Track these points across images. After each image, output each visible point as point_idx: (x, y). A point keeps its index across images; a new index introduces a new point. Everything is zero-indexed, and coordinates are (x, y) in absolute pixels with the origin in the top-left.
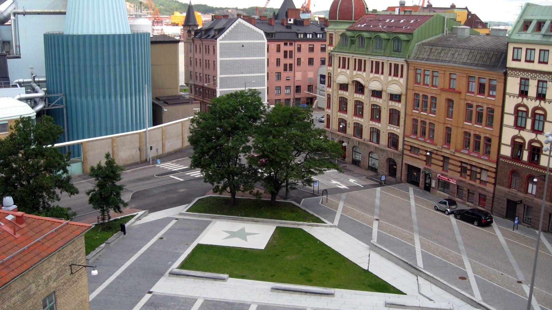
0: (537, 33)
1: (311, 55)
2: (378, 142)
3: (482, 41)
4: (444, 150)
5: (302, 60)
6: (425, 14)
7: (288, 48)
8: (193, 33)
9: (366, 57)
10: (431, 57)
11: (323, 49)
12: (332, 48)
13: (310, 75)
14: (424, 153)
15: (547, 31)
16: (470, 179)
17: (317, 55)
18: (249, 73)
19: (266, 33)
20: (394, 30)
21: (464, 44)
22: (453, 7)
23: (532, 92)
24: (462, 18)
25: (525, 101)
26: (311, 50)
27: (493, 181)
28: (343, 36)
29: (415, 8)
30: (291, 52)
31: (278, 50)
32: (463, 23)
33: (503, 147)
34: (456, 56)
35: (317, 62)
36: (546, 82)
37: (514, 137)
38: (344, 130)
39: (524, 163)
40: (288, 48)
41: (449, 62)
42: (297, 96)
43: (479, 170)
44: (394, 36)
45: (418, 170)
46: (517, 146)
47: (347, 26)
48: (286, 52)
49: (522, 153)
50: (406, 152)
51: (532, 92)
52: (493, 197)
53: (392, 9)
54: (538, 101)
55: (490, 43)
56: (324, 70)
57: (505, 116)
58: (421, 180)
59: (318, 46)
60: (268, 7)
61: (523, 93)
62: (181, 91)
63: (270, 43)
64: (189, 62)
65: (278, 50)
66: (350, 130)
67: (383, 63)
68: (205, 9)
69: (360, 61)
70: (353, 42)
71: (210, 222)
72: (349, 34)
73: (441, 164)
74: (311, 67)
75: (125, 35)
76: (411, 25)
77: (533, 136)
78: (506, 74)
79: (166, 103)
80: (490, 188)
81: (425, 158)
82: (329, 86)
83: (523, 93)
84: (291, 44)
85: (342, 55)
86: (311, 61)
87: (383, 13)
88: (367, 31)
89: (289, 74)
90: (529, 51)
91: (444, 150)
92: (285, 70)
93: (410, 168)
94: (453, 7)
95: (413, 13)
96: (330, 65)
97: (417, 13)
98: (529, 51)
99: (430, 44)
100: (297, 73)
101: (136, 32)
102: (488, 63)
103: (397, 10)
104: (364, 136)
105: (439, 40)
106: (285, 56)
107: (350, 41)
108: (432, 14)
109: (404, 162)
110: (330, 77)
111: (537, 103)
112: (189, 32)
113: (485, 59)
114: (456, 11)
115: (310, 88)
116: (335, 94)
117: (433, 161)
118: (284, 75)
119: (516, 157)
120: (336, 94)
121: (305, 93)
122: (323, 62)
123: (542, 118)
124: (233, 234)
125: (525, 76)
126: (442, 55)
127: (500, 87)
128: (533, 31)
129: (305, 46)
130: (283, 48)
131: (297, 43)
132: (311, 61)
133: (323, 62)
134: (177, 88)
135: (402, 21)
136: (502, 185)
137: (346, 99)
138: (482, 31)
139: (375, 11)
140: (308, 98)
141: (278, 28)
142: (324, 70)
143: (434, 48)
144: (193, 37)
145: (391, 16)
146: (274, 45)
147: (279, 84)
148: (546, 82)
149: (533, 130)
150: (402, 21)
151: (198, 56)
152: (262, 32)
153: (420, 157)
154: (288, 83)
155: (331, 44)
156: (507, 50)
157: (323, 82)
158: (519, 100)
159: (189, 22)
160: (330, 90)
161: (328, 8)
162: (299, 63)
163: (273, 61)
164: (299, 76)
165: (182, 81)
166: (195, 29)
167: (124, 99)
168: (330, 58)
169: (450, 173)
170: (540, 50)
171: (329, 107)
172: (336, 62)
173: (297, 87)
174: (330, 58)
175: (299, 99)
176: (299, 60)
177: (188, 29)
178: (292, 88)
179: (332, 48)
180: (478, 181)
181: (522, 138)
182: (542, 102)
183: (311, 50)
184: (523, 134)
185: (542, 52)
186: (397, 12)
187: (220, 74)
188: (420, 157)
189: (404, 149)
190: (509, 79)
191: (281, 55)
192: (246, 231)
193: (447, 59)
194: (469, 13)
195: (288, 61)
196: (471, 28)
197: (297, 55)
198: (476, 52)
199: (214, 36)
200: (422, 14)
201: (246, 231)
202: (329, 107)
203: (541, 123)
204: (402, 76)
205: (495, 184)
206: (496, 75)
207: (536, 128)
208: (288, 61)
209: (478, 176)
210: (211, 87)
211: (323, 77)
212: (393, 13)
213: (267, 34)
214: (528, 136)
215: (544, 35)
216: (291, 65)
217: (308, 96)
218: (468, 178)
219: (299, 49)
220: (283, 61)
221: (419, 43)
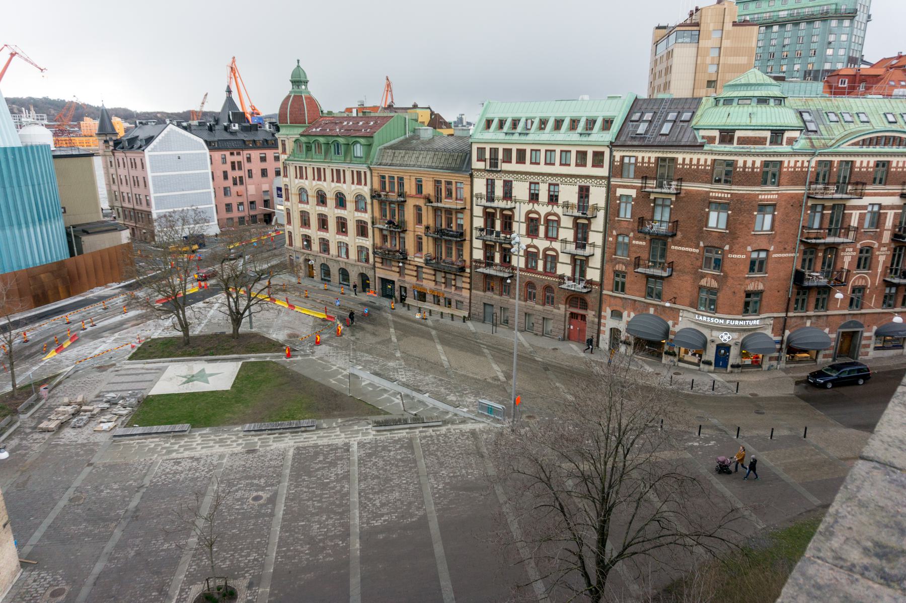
0: (572, 132)
1: (264, 165)
2: (348, 257)
3: (446, 142)
4: (416, 259)
5: (254, 172)
6: (385, 115)
7: (236, 158)
8: (111, 143)
9: (325, 165)
10: (394, 162)
11: (277, 159)
12: (285, 157)
13: (265, 187)
14: (396, 264)
15: (509, 128)
16: (446, 287)
17: (271, 166)
18: (191, 189)
19: (206, 141)
20: (353, 133)
21: (428, 146)
22: (415, 106)
23: (543, 196)
24: (425, 117)
25: (537, 207)
26: (263, 159)
27: (468, 286)
28: (296, 141)
29: (375, 108)
30: (239, 163)
31: (224, 162)
32: (426, 124)
33: (475, 251)
34: (420, 159)
35: (271, 173)
36: (558, 185)
37: (528, 246)
38: (309, 246)
39: (539, 273)
40: (236, 158)
41: (414, 166)
42: (253, 213)
43: (453, 277)
44: (354, 140)
45: (393, 282)
46: (531, 256)
47: (301, 130)
48: (233, 163)
49: (536, 263)
50: (378, 265)
51: (543, 196)
52: (470, 303)
53: (349, 110)
54: (550, 206)
55: (454, 144)
56: (281, 181)
57: (474, 218)
58: (397, 294)
59: (270, 154)
60: (206, 109)
61: (534, 198)
62: (104, 216)
63: (212, 153)
64: (112, 181)
65: (224, 162)
66: (316, 247)
67: (344, 171)
68: (127, 115)
69: (338, 171)
70: (309, 149)
71: (167, 367)
72: (303, 139)
73: (415, 274)
74: (265, 179)
75: (13, 149)
76: (371, 128)
77: (547, 244)
78: (471, 176)
79: (86, 232)
80: (466, 293)
81: (397, 270)
82: (287, 199)
83: (534, 198)
84: (238, 154)
85: (298, 164)
86: (264, 173)
87: (339, 115)
88: (323, 136)
89: (239, 188)
90: (534, 153)
91: (416, 259)
92: (235, 184)
93: (385, 282)
94: (415, 106)
95: (372, 115)
96: (285, 176)
97: (377, 115)
98: (564, 154)
99: (392, 147)
100: (249, 187)
101: (29, 144)
102: (453, 165)
103: (354, 111)
104: (331, 252)
105: (402, 142)
106: (233, 168)
107: (307, 147)
108: (392, 114)
109: (377, 275)
110: (287, 190)
111: (549, 209)
112: (106, 142)
113: (450, 161)
114: (418, 111)
115: (266, 203)
116: (295, 208)
117: (407, 272)
118: (234, 189)
119: (530, 268)
120: (297, 208)
121: (261, 209)
122: (278, 173)
123: (555, 225)
124: (190, 379)
125: (554, 182)
126: (406, 159)
127: (467, 188)
128: (496, 129)
129: (255, 154)
130: (230, 159)
131: (245, 152)
132: (264, 173)
133: (278, 173)
134: (97, 212)
135: (361, 123)
136: (477, 289)
137: (326, 216)
138: (445, 132)
139: (330, 113)
140: (265, 215)
141: (220, 135)
142: (281, 181)
143: (397, 152)
144: (112, 148)
145: (349, 118)
146: (218, 155)
147: (228, 200)
148: (558, 185)
149: (547, 237)
150: (361, 123)
151: (122, 172)
152: (202, 141)
153: (394, 269)
154: (240, 200)
155: (284, 152)
156: (471, 151)
157: (280, 196)
158: (530, 207)
159: (106, 129)
160: (288, 204)
161: (277, 111)
162: (250, 176)
163: (219, 174)
164: (252, 189)
165: (105, 204)
166: (114, 138)
167: (24, 230)
168: (285, 168)
169: (407, 278)
170: (546, 151)
171: (289, 222)
172: (291, 171)
173: (252, 203)
174: (285, 168)
175: (256, 216)
176: (250, 171)
177: (104, 138)
178: (246, 204)
179: (285, 157)
180: (453, 288)
181: (535, 247)
182: (555, 207)
183: (263, 159)
184: (536, 242)
185: (548, 153)
186: (354, 114)
187: (155, 192)
188: (394, 269)
189: (375, 262)
190: (475, 180)
191: (228, 167)
192: (207, 372)
193: (412, 163)
194: (432, 113)
195: (237, 173)
196: (435, 128)
197: (247, 166)
198: (440, 154)
199: (140, 147)
200: (382, 115)
201: (207, 372)
202: (289, 222)
203: (555, 229)
204: (365, 184)
205: (470, 289)
206: (463, 178)
207: (550, 235)
208: (237, 173)
209: (453, 283)
210: (144, 207)
211: (279, 189)
212: (350, 115)
213: (208, 143)
214: (542, 244)
215: (506, 134)
216: (241, 178)
217: (265, 212)
218: (443, 285)
219: (249, 160)
220: (232, 174)
221: (381, 147)
